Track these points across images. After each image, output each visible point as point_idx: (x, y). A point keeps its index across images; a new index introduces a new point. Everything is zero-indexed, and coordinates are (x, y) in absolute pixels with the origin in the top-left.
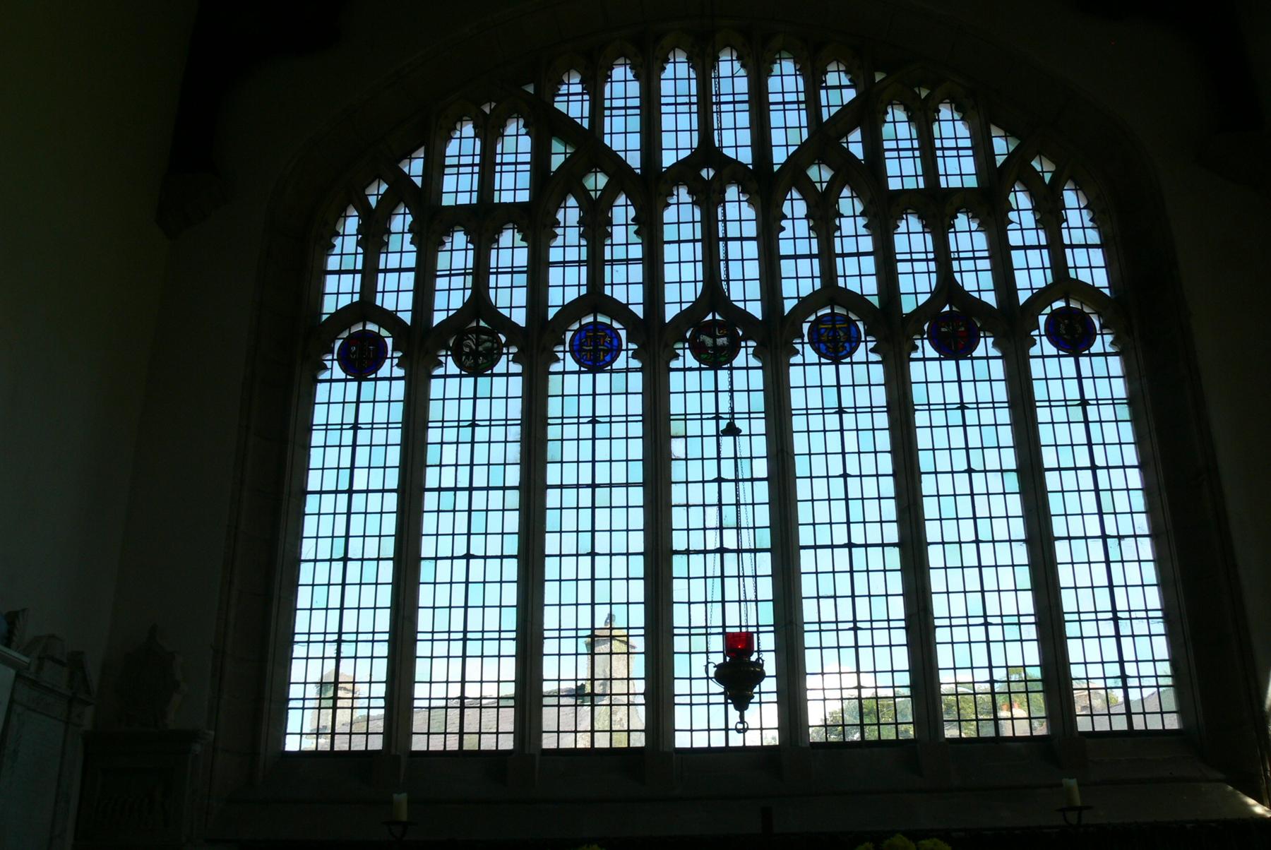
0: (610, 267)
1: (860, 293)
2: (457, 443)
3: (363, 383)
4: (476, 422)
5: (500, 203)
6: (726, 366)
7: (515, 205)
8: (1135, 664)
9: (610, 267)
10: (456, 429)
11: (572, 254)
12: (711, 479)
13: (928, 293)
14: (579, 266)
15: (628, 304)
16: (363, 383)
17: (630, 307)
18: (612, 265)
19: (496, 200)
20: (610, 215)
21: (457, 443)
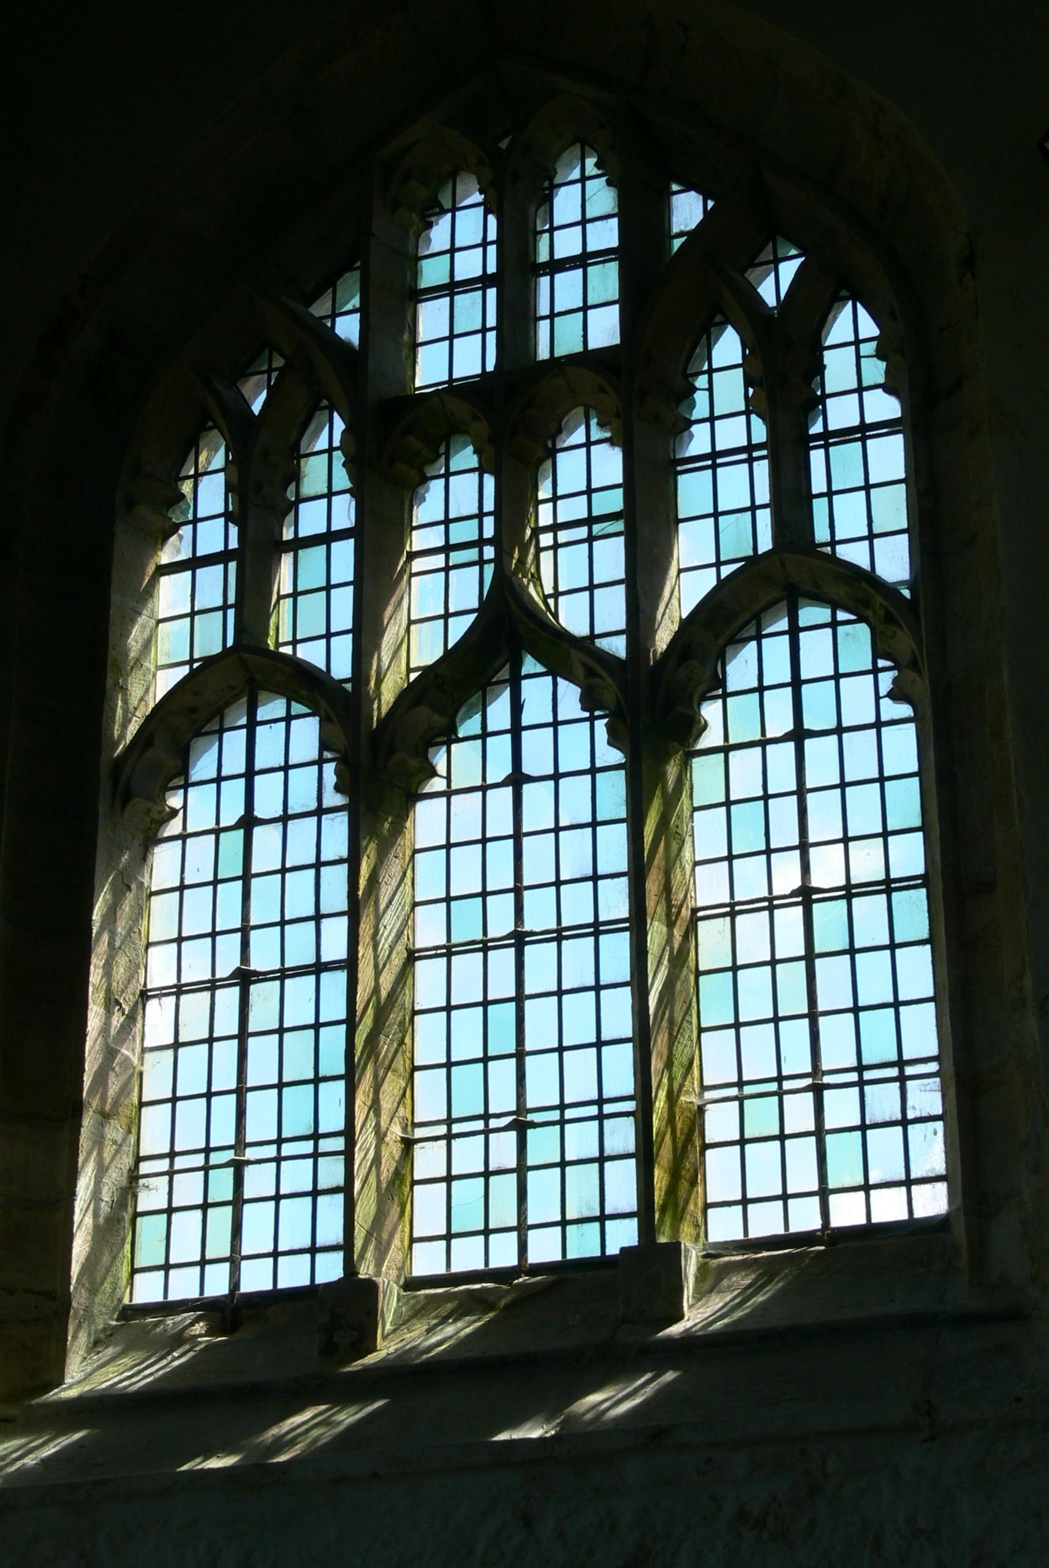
0: (822, 451)
1: (560, 680)
2: (904, 1122)
3: (822, 431)
4: (800, 899)
5: (553, 360)
6: (714, 693)
7: (587, 358)
8: (724, 853)
9: (822, 451)
10: (906, 1056)
11: (732, 434)
12: (499, 780)
13: (555, 685)
14: (750, 461)
15: (593, 636)
16: (822, 431)
17: (599, 643)
18: (826, 447)
19: (543, 354)
20: (751, 391)
21: (904, 1122)
